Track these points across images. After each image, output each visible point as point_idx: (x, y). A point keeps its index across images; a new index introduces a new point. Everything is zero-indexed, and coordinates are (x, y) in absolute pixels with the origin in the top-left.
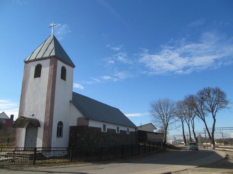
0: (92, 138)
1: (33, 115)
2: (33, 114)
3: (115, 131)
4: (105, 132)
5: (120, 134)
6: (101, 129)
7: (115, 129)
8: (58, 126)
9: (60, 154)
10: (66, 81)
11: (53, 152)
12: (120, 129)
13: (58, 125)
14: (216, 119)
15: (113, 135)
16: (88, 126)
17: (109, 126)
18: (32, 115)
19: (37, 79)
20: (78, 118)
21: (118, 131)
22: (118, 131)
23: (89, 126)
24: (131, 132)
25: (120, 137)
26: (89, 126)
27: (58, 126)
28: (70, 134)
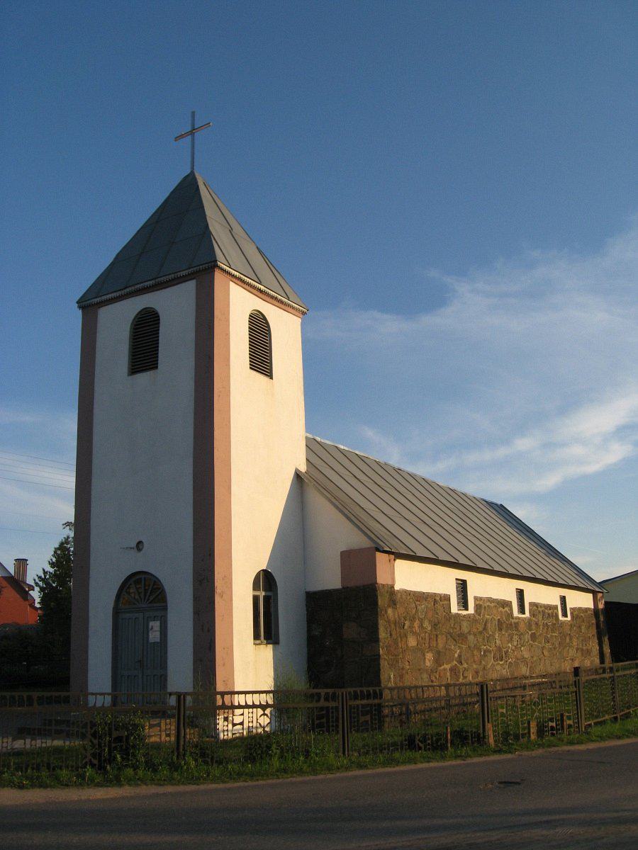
0: (412, 642)
1: (139, 545)
2: (140, 543)
3: (507, 609)
4: (465, 613)
5: (529, 623)
6: (447, 598)
7: (507, 599)
8: (257, 593)
9: (242, 724)
10: (272, 378)
11: (260, 711)
12: (528, 599)
13: (254, 589)
14: (499, 503)
15: (500, 630)
16: (392, 587)
17: (483, 587)
18: (134, 544)
19: (143, 378)
20: (342, 553)
21: (464, 603)
22: (464, 603)
23: (397, 587)
24: (578, 613)
25: (533, 637)
26: (397, 587)
27: (257, 593)
28: (309, 630)
